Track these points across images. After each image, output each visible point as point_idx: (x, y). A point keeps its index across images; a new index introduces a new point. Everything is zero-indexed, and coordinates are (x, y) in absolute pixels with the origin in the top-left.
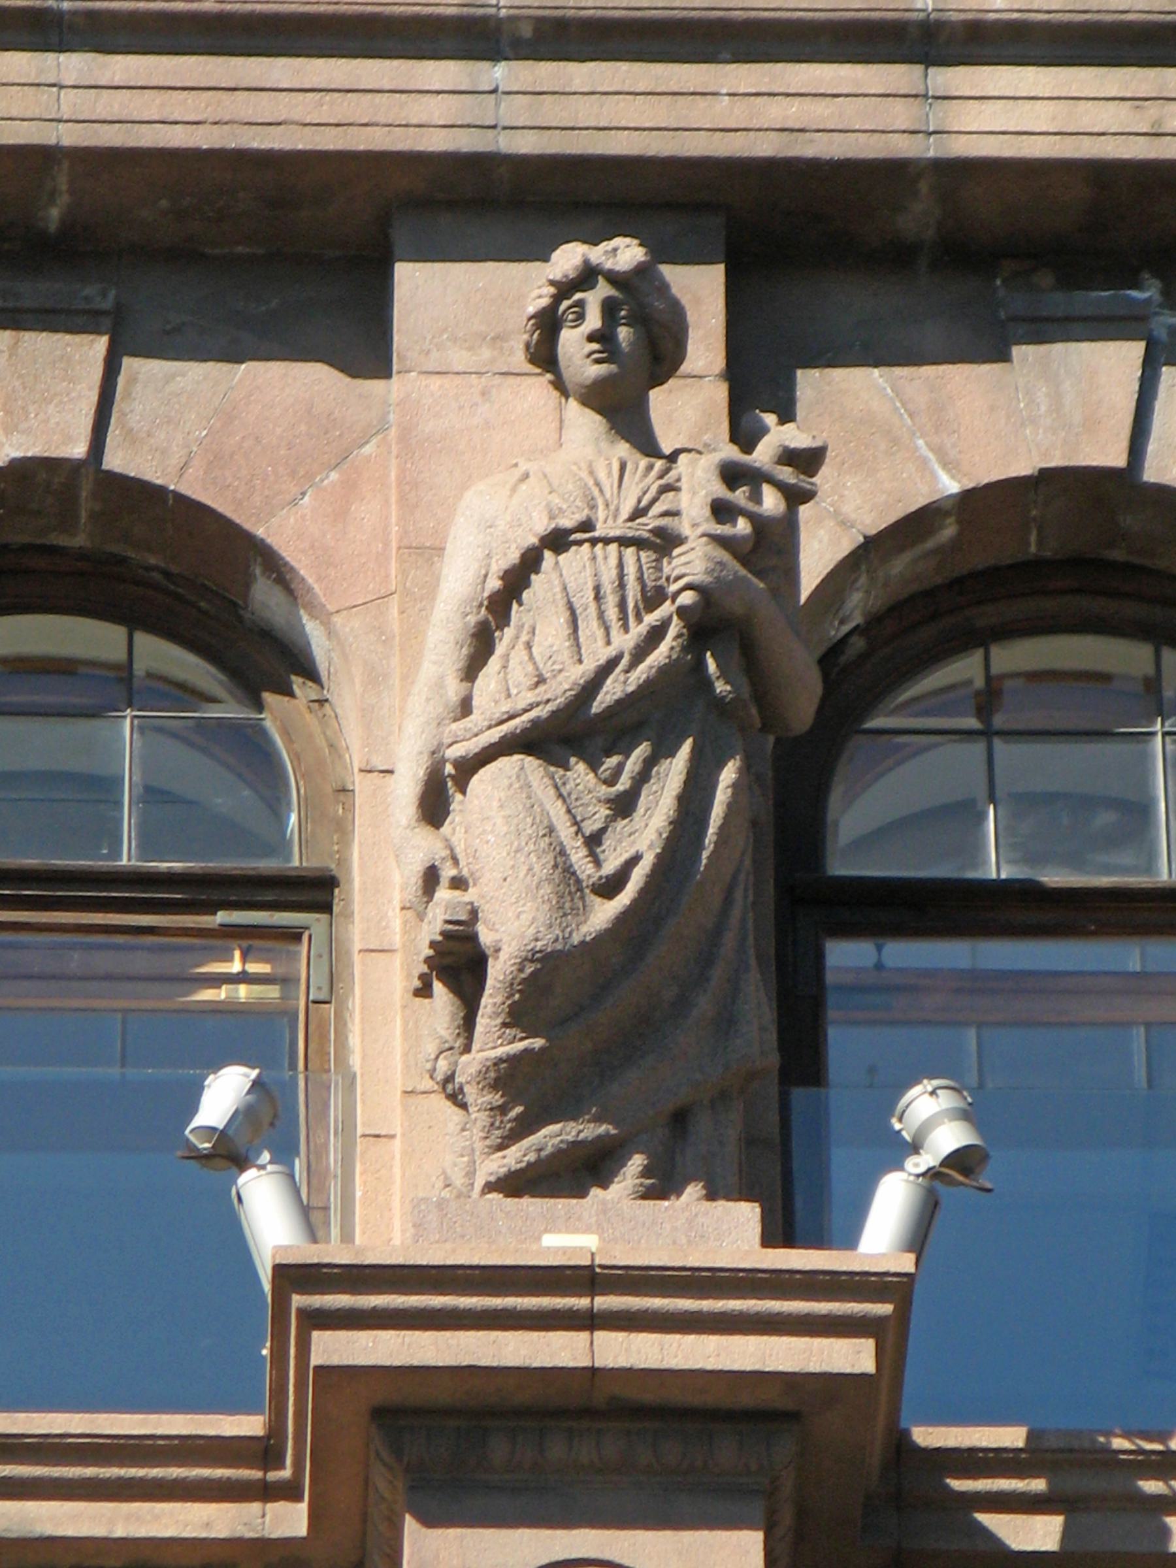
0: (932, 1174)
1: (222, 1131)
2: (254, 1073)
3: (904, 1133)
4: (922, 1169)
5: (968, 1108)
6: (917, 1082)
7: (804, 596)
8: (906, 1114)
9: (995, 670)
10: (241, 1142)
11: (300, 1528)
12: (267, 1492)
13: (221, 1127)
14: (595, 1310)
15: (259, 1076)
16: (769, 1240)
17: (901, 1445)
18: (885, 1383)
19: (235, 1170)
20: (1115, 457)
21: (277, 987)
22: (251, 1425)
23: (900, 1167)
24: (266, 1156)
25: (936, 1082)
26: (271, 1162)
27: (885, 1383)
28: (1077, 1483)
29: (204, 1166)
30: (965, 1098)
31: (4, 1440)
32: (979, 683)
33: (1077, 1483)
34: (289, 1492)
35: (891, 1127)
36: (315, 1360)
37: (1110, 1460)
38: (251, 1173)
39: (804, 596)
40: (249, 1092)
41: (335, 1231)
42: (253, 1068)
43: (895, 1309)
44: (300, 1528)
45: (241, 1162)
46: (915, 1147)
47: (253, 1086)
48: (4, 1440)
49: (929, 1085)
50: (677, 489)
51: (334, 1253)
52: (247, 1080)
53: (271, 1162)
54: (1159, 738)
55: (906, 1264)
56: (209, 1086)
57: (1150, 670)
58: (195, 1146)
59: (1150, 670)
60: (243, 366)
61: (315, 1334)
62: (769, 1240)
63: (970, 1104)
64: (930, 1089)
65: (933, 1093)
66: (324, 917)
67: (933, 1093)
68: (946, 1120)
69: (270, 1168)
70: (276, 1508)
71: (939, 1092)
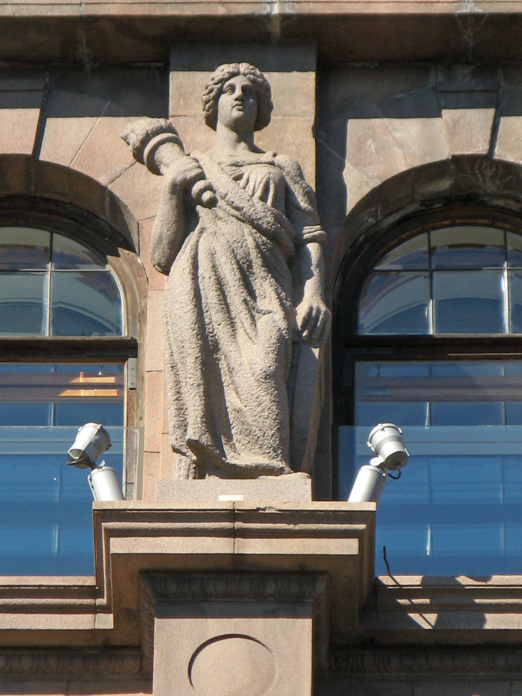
0: (381, 466)
1: (83, 451)
2: (99, 426)
3: (372, 448)
4: (378, 464)
5: (399, 435)
6: (376, 425)
7: (347, 214)
8: (372, 439)
9: (432, 245)
10: (91, 455)
11: (110, 625)
12: (93, 610)
13: (83, 450)
14: (235, 528)
15: (101, 427)
16: (317, 496)
17: (378, 586)
18: (366, 556)
19: (90, 468)
20: (482, 149)
21: (115, 390)
22: (90, 581)
23: (368, 463)
24: (103, 463)
25: (384, 425)
26: (105, 466)
27: (366, 556)
28: (445, 600)
29: (76, 466)
30: (399, 431)
31: (1, 588)
32: (425, 248)
33: (445, 600)
34: (104, 609)
35: (367, 445)
36: (111, 552)
37: (460, 589)
38: (96, 470)
39: (347, 214)
40: (96, 435)
41: (135, 494)
42: (99, 424)
43: (367, 526)
44: (110, 625)
45: (93, 466)
46: (376, 454)
47: (98, 432)
48: (1, 588)
49: (380, 426)
50: (167, 167)
51: (132, 504)
52: (96, 429)
53: (105, 466)
54: (49, 273)
55: (372, 506)
56: (80, 431)
57: (502, 243)
58: (72, 458)
59: (48, 245)
60: (100, 118)
61: (112, 539)
62: (317, 496)
63: (401, 434)
64: (381, 428)
65: (383, 429)
66: (136, 359)
67: (383, 429)
68: (388, 441)
69: (104, 468)
70: (101, 616)
71: (385, 429)
